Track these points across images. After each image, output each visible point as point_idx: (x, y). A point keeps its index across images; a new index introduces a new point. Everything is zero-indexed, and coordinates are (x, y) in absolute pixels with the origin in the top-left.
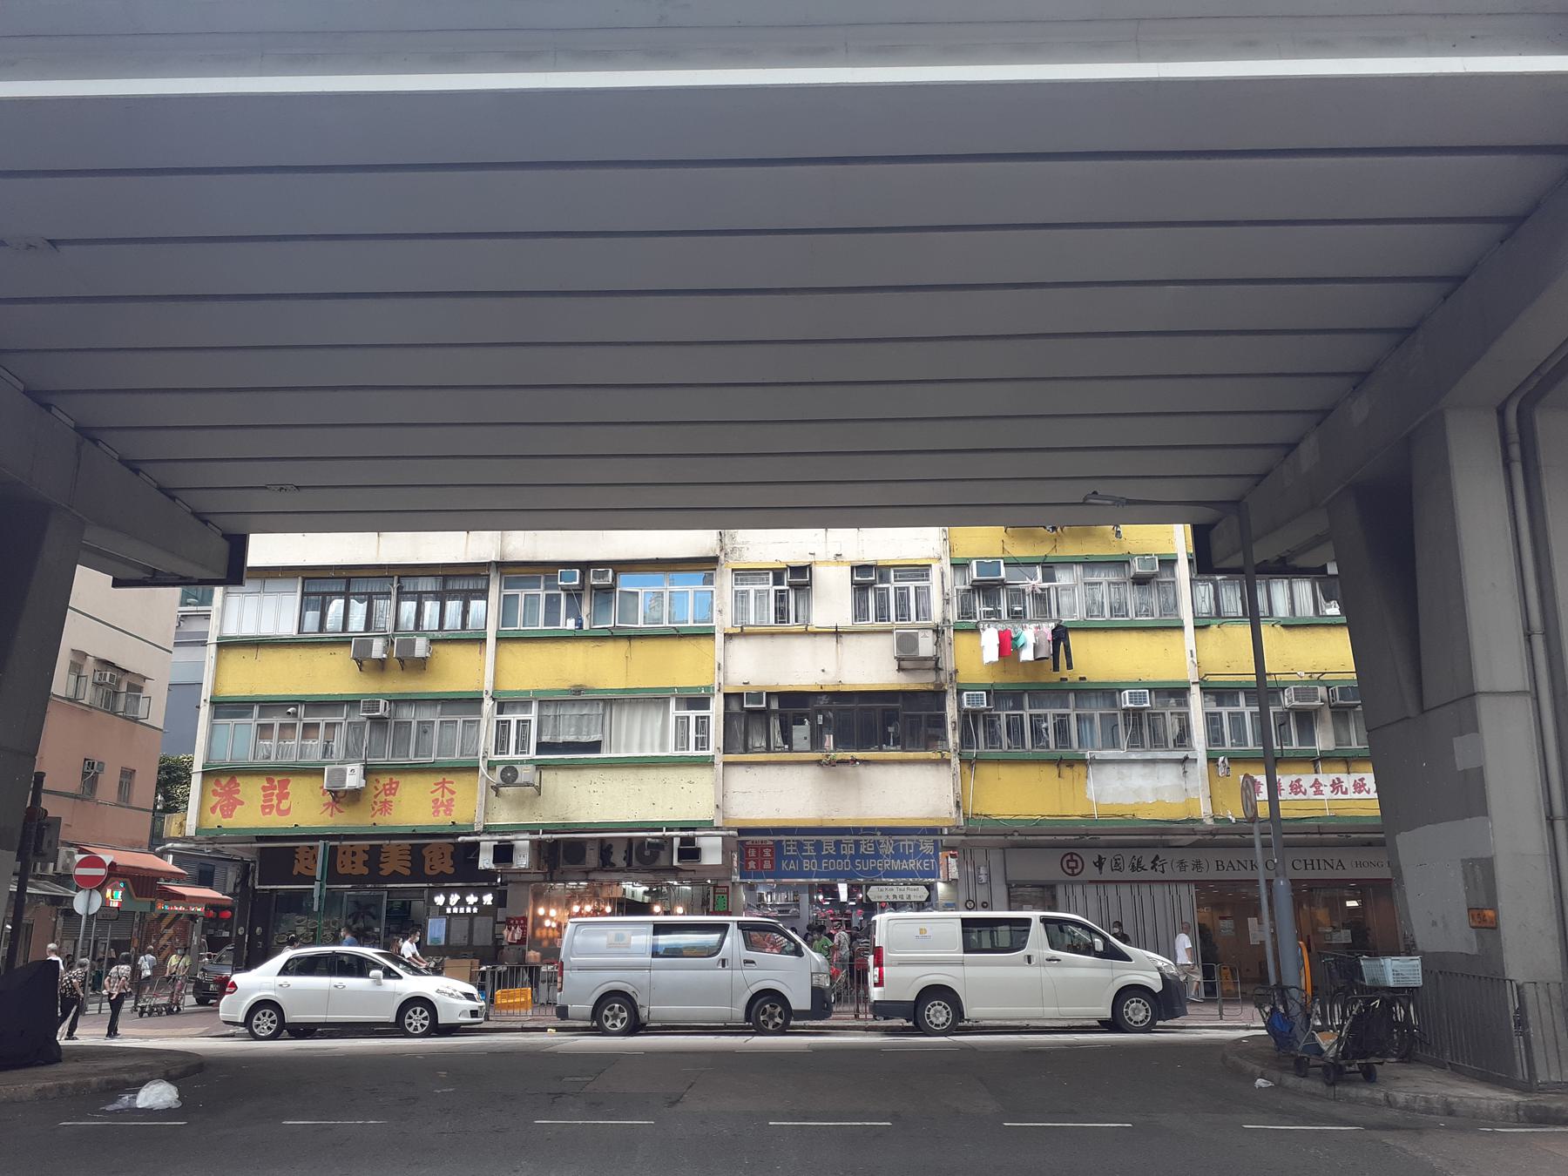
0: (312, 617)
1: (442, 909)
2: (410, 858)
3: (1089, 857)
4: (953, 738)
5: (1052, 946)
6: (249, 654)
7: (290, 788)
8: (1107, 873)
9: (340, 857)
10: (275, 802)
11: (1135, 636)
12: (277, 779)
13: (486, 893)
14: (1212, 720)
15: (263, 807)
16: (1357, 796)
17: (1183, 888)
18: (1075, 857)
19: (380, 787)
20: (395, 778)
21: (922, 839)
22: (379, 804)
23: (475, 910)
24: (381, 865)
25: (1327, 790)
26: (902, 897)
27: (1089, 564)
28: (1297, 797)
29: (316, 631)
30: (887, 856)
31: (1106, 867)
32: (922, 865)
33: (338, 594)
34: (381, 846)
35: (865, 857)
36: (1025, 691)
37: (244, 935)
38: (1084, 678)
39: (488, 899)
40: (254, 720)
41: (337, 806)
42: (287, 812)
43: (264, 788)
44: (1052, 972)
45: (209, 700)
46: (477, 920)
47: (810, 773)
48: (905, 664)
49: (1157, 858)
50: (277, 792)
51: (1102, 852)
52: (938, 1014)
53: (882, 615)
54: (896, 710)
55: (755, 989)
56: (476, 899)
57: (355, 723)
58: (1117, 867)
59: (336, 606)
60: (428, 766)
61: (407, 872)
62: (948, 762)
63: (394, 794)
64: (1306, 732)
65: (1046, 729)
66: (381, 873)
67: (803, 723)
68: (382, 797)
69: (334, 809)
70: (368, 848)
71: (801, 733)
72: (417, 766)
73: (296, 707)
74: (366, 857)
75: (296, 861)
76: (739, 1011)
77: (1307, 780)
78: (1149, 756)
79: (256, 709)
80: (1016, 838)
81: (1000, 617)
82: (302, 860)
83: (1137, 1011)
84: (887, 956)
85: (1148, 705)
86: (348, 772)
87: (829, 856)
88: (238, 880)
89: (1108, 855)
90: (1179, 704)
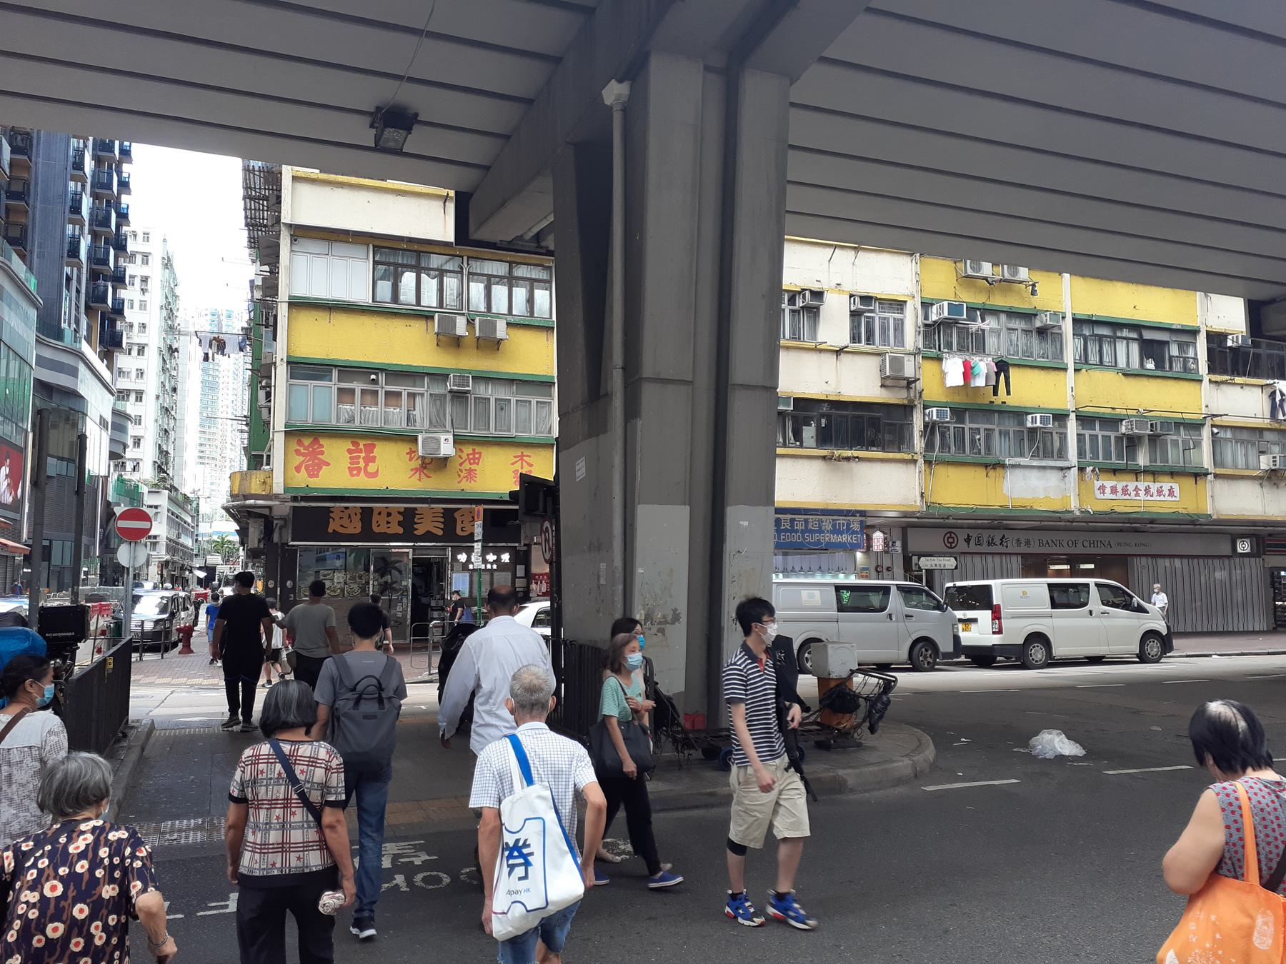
0: (385, 288)
1: (465, 567)
2: (442, 520)
3: (962, 535)
4: (919, 443)
5: (1103, 604)
6: (322, 316)
7: (376, 452)
8: (973, 547)
9: (375, 518)
10: (362, 465)
11: (1036, 372)
12: (362, 443)
13: (504, 553)
14: (1080, 438)
15: (351, 470)
16: (1158, 498)
17: (1014, 558)
18: (953, 535)
19: (464, 456)
20: (478, 449)
21: (851, 519)
22: (465, 472)
23: (495, 567)
24: (415, 526)
25: (1142, 493)
26: (940, 565)
27: (1012, 314)
28: (1125, 497)
29: (389, 301)
30: (828, 531)
31: (972, 542)
32: (852, 538)
33: (410, 267)
34: (416, 509)
35: (812, 532)
36: (966, 409)
37: (275, 587)
38: (1005, 403)
39: (506, 557)
40: (334, 384)
41: (425, 471)
42: (375, 474)
43: (349, 451)
44: (1105, 622)
45: (285, 360)
46: (496, 574)
47: (818, 465)
48: (888, 383)
49: (1004, 537)
50: (363, 455)
51: (971, 532)
52: (1037, 653)
53: (869, 340)
54: (879, 418)
55: (915, 637)
56: (495, 557)
57: (436, 395)
58: (979, 543)
59: (408, 278)
60: (510, 440)
61: (440, 533)
62: (915, 462)
63: (478, 464)
64: (1132, 454)
65: (979, 440)
66: (415, 532)
67: (810, 425)
68: (467, 466)
69: (422, 475)
70: (402, 510)
71: (809, 433)
72: (498, 440)
73: (376, 374)
74: (401, 518)
75: (331, 520)
76: (903, 654)
77: (1154, 487)
78: (1044, 463)
79: (335, 373)
80: (951, 521)
81: (952, 349)
82: (337, 519)
83: (1154, 648)
84: (1003, 612)
85: (1051, 426)
86: (442, 441)
87: (786, 530)
88: (262, 536)
89: (974, 533)
90: (1060, 426)
